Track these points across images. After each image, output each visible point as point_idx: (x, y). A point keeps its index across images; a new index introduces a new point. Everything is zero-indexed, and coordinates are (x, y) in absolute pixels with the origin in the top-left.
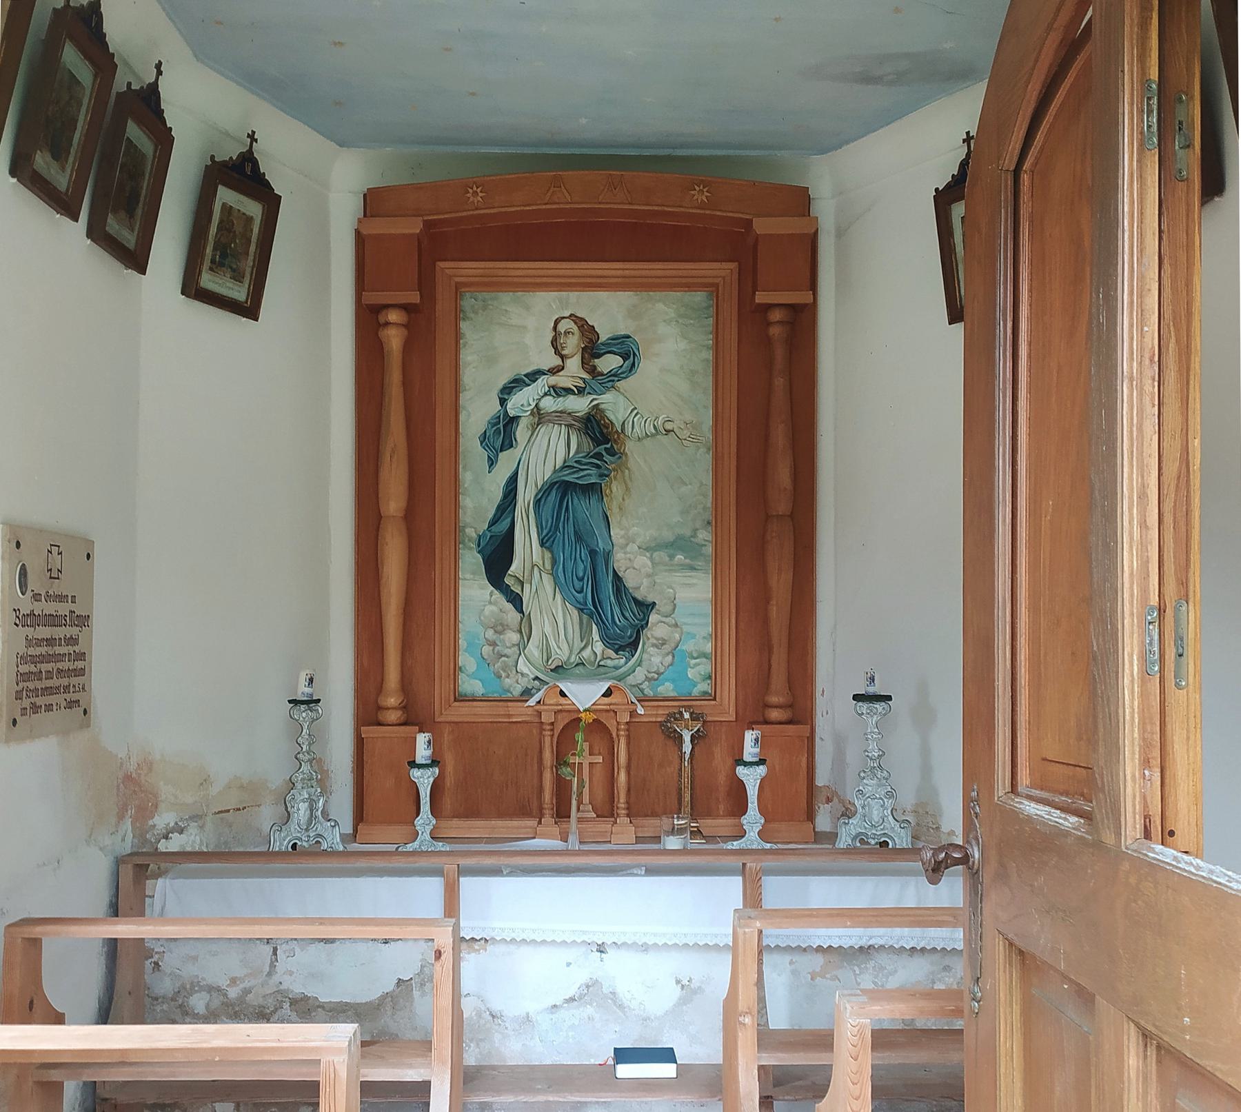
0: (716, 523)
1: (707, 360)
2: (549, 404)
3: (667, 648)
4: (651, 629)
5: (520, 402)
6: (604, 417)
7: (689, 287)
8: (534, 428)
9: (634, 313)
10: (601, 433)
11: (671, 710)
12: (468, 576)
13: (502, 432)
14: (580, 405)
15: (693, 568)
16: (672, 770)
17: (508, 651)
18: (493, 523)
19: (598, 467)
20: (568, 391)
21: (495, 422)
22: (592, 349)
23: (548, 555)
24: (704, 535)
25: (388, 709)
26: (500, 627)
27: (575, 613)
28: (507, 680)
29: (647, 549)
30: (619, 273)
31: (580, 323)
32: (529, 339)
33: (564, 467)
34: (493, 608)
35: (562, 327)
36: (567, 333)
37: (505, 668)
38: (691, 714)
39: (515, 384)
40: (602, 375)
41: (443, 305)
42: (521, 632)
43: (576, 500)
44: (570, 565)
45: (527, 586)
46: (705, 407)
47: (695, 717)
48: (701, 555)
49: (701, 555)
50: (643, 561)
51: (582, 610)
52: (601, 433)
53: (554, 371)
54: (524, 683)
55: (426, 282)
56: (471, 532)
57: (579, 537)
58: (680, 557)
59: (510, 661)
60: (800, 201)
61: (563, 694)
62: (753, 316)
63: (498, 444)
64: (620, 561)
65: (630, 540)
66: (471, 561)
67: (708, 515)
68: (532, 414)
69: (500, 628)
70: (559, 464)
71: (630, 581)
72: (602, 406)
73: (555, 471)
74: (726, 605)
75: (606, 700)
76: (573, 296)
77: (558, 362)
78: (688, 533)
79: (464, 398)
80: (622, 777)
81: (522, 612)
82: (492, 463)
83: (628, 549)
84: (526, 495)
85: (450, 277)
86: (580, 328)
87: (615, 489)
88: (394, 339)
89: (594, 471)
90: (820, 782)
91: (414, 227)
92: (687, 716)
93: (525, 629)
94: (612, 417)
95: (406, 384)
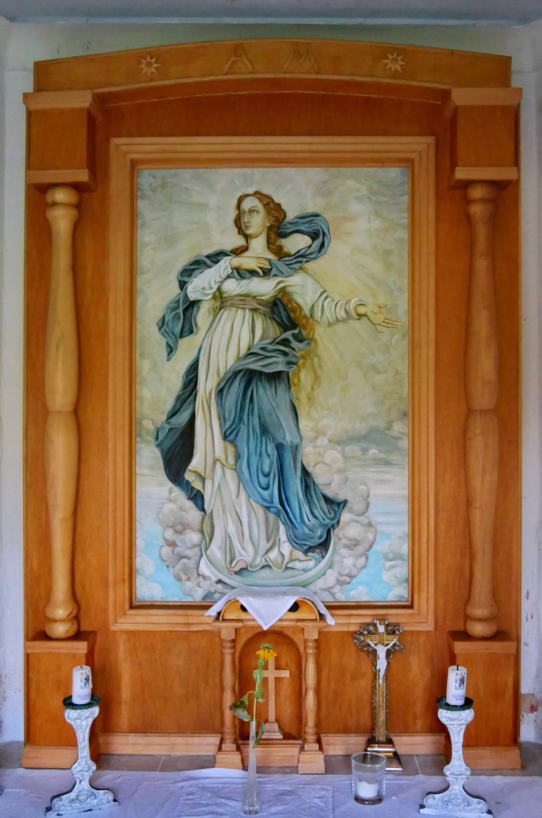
0: (411, 415)
1: (402, 240)
2: (232, 287)
3: (360, 549)
4: (342, 528)
5: (201, 285)
6: (291, 300)
7: (382, 162)
8: (216, 312)
9: (323, 190)
10: (289, 318)
11: (368, 620)
12: (146, 471)
13: (183, 316)
14: (265, 288)
15: (387, 463)
16: (365, 683)
17: (189, 553)
18: (173, 414)
19: (285, 354)
20: (253, 273)
21: (174, 307)
22: (278, 228)
23: (231, 449)
24: (400, 428)
25: (55, 621)
26: (180, 527)
27: (260, 512)
28: (188, 584)
29: (339, 442)
30: (306, 147)
31: (266, 201)
32: (211, 218)
33: (250, 354)
34: (172, 506)
35: (247, 204)
36: (251, 211)
37: (186, 570)
38: (387, 626)
39: (197, 266)
40: (290, 256)
41: (117, 181)
42: (202, 531)
43: (261, 390)
44: (254, 460)
45: (208, 483)
46: (400, 289)
47: (392, 630)
48: (397, 449)
49: (397, 449)
50: (333, 455)
51: (268, 508)
52: (289, 318)
53: (238, 252)
54: (206, 586)
55: (96, 160)
56: (148, 425)
57: (265, 430)
58: (373, 451)
59: (191, 563)
60: (500, 70)
61: (243, 609)
62: (453, 193)
63: (177, 330)
64: (309, 455)
65: (319, 433)
66: (149, 458)
67: (404, 406)
68: (214, 298)
69: (179, 528)
70: (244, 350)
71: (320, 476)
72: (289, 289)
73: (239, 359)
74: (424, 512)
75: (293, 616)
76: (258, 173)
77: (240, 241)
78: (382, 425)
79: (141, 281)
80: (310, 699)
81: (203, 509)
82: (171, 350)
83: (318, 442)
84: (207, 385)
85: (126, 153)
86: (266, 206)
87: (305, 377)
88: (62, 221)
89: (281, 359)
90: (525, 689)
91: (82, 100)
92: (381, 629)
93: (207, 534)
94: (300, 301)
95: (75, 268)
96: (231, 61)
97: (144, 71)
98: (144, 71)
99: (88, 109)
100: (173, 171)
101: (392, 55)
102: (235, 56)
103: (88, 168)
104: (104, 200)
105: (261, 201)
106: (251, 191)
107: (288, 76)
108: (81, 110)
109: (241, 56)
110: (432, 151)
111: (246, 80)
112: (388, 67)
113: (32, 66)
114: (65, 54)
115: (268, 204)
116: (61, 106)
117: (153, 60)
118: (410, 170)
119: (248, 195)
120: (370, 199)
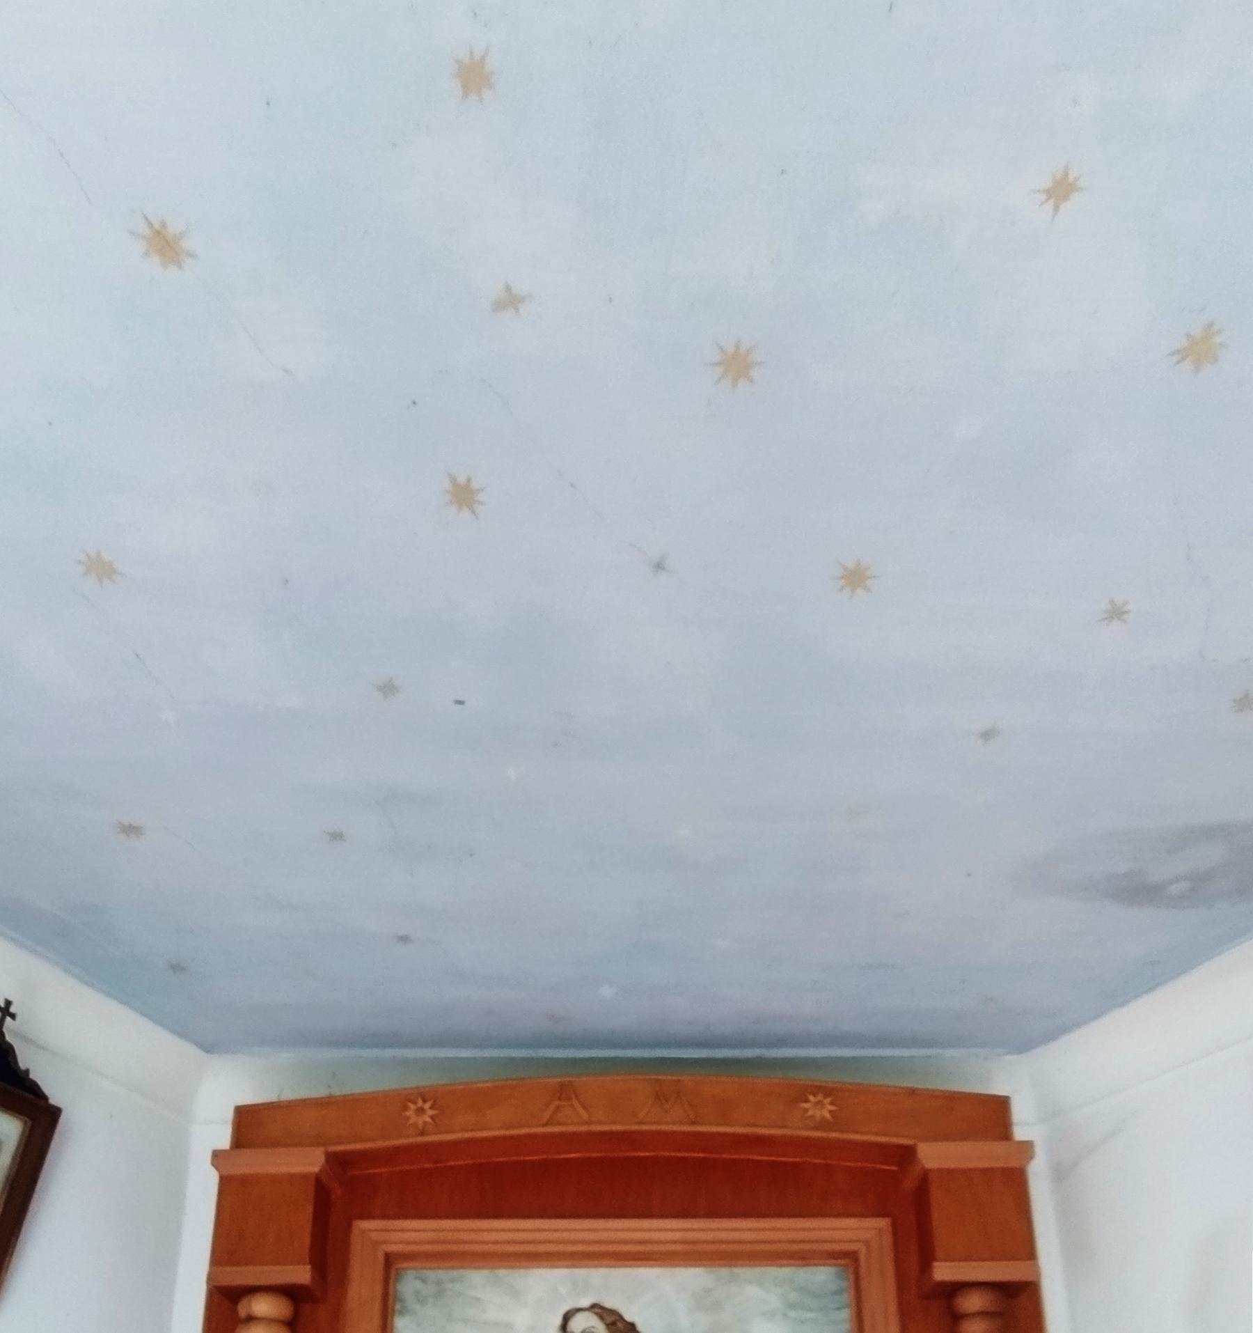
7: (801, 1257)
31: (610, 1319)
35: (578, 1323)
41: (361, 1287)
55: (328, 1252)
60: (993, 1115)
85: (377, 1244)
91: (311, 1162)
96: (552, 1107)
97: (412, 1121)
98: (412, 1121)
99: (318, 1179)
100: (455, 1273)
101: (815, 1095)
102: (560, 1099)
103: (311, 1263)
104: (337, 1314)
105: (601, 1318)
106: (585, 1303)
107: (644, 1128)
108: (304, 1176)
109: (569, 1099)
110: (888, 1240)
111: (575, 1134)
112: (810, 1113)
113: (230, 1115)
114: (289, 1095)
115: (613, 1324)
116: (272, 1170)
117: (427, 1106)
118: (851, 1270)
119: (579, 1310)
120: (785, 1315)
